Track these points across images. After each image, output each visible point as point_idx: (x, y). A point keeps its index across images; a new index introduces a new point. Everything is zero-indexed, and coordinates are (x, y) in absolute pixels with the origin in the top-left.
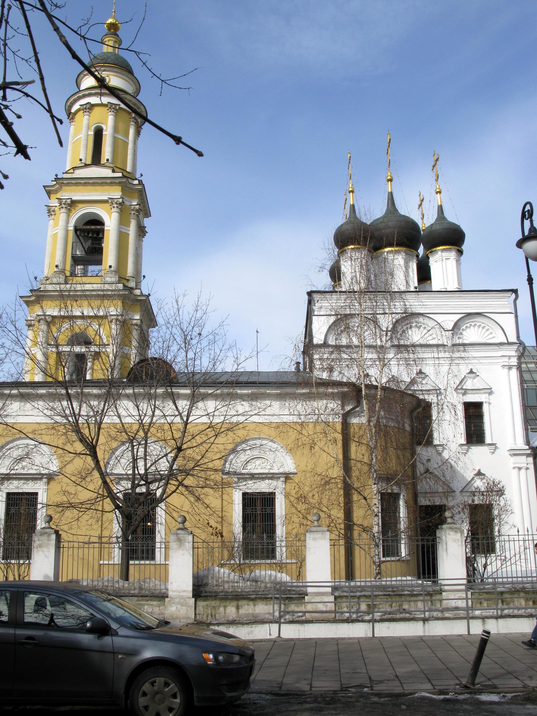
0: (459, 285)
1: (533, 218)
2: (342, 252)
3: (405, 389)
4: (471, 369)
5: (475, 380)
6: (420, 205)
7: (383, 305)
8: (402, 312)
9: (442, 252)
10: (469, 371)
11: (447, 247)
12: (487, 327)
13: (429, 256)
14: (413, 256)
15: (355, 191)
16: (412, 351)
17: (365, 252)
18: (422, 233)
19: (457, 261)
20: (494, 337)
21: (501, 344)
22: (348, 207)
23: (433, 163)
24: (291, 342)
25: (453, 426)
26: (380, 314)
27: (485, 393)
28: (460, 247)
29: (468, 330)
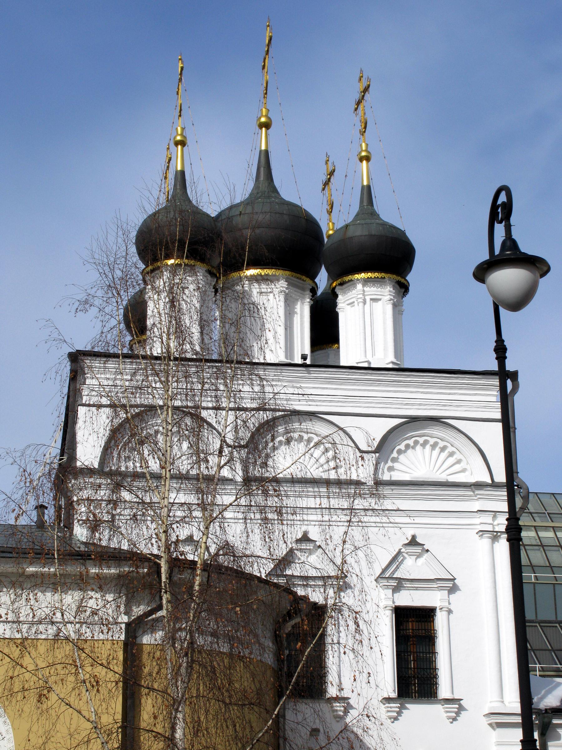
0: (396, 356)
1: (513, 220)
2: (152, 271)
3: (269, 574)
4: (414, 537)
5: (421, 561)
6: (326, 183)
7: (217, 390)
8: (254, 405)
9: (364, 286)
10: (300, 536)
11: (377, 275)
12: (450, 449)
13: (337, 291)
14: (303, 289)
15: (189, 142)
16: (275, 491)
17: (201, 275)
18: (326, 240)
19: (395, 306)
20: (464, 470)
21: (479, 485)
22: (171, 175)
23: (357, 96)
24: (11, 460)
25: (351, 655)
26: (207, 408)
27: (441, 588)
28: (404, 278)
29: (410, 451)
